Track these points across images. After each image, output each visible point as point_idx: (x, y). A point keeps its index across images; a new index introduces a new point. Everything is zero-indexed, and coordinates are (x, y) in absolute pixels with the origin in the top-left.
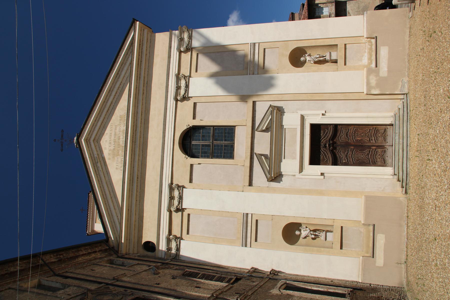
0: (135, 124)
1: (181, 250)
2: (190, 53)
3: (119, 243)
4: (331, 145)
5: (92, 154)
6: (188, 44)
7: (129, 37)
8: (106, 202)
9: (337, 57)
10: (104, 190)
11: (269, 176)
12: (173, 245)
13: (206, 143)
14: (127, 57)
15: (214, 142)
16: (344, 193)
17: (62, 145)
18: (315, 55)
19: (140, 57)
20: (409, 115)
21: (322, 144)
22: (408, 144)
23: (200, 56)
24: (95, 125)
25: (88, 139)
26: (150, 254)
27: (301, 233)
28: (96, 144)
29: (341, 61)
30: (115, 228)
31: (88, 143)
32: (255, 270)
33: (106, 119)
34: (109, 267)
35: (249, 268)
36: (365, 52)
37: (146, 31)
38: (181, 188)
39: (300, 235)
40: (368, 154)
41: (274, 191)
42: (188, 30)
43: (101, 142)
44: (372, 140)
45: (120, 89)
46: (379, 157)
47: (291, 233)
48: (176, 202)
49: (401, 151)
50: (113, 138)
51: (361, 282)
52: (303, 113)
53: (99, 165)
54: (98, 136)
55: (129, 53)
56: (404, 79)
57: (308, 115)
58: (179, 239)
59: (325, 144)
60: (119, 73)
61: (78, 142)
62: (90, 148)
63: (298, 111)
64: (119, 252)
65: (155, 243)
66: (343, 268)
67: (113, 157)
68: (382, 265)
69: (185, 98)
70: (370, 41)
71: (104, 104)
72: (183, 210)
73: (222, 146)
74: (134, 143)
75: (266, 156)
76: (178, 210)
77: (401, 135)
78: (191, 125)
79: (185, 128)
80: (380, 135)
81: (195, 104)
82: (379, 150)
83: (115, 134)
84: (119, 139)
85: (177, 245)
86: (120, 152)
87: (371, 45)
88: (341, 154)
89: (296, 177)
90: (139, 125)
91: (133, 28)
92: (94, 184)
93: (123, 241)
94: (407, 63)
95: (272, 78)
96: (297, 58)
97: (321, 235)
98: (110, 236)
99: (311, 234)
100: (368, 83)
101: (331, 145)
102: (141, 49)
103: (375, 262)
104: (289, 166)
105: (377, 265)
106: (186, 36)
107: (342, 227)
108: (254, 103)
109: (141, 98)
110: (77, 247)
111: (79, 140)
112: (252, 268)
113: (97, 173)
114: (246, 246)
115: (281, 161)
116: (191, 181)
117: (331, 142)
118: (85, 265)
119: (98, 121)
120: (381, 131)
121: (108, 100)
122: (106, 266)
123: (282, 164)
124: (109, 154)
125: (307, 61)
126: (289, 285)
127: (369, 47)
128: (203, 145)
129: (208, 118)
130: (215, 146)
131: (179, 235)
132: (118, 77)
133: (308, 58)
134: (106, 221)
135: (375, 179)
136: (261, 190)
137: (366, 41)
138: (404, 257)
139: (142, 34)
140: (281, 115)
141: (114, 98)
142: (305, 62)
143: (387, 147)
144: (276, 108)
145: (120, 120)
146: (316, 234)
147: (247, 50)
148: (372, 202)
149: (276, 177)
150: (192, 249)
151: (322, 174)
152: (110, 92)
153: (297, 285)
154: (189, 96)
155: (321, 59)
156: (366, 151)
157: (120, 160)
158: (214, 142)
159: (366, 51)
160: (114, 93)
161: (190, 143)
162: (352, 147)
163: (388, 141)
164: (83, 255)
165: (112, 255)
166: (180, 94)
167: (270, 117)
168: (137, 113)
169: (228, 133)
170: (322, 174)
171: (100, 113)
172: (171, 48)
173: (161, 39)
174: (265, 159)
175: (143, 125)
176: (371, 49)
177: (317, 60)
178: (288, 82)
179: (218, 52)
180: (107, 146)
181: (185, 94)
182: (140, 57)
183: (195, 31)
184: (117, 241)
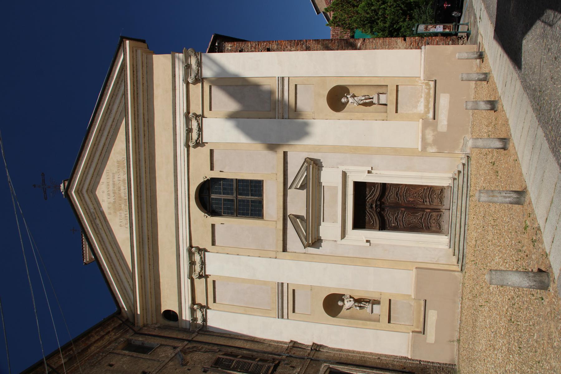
0: (138, 174)
1: (208, 320)
3: (134, 314)
4: (380, 206)
5: (87, 208)
6: (197, 74)
7: (118, 62)
8: (113, 267)
10: (108, 251)
11: (306, 243)
12: (199, 315)
13: (229, 197)
14: (118, 86)
15: (238, 196)
16: (393, 262)
18: (361, 94)
19: (135, 88)
20: (469, 189)
21: (368, 204)
22: (466, 223)
23: (213, 89)
24: (86, 173)
25: (80, 190)
26: (172, 323)
27: (344, 304)
28: (91, 195)
29: (391, 107)
30: (127, 296)
31: (81, 195)
32: (294, 345)
33: (99, 165)
34: (129, 356)
35: (288, 340)
36: (421, 97)
37: (139, 52)
40: (421, 218)
42: (195, 55)
43: (97, 193)
44: (426, 201)
45: (114, 127)
46: (434, 221)
48: (198, 268)
49: (459, 213)
50: (111, 188)
52: (344, 168)
53: (98, 221)
54: (92, 185)
55: (120, 82)
56: (466, 136)
57: (351, 172)
58: (204, 308)
59: (372, 205)
60: (110, 107)
61: (67, 189)
62: (83, 201)
63: (340, 167)
64: (136, 325)
65: (177, 312)
66: (392, 343)
67: (115, 212)
68: (433, 342)
69: (199, 144)
70: (428, 83)
71: (95, 147)
72: (207, 277)
73: (248, 201)
74: (139, 198)
76: (200, 277)
77: (459, 208)
78: (208, 178)
79: (202, 180)
80: (435, 196)
81: (212, 151)
82: (434, 214)
83: (114, 184)
84: (120, 190)
85: (203, 315)
86: (123, 206)
87: (429, 89)
88: (390, 217)
89: (338, 243)
90: (143, 175)
91: (121, 49)
92: (95, 246)
93: (139, 313)
94: (471, 117)
95: (306, 124)
96: (337, 98)
98: (123, 306)
99: (356, 306)
100: (424, 139)
101: (380, 206)
102: (135, 77)
103: (426, 339)
104: (329, 230)
105: (428, 341)
106: (193, 61)
107: (390, 300)
108: (285, 154)
109: (142, 141)
110: (87, 334)
111: (69, 192)
112: (291, 341)
113: (97, 232)
114: (283, 317)
115: (319, 224)
116: (213, 243)
117: (378, 203)
118: (100, 358)
119: (90, 168)
120: (437, 192)
121: (99, 142)
122: (124, 355)
123: (321, 228)
124: (109, 208)
126: (333, 370)
127: (427, 91)
128: (225, 200)
129: (231, 170)
130: (240, 201)
131: (204, 304)
132: (108, 112)
134: (115, 290)
136: (297, 257)
137: (423, 83)
138: (457, 335)
139: (135, 57)
140: (319, 170)
141: (107, 138)
143: (443, 210)
144: (312, 162)
145: (119, 166)
146: (362, 305)
147: (273, 85)
148: (424, 272)
152: (101, 132)
153: (340, 369)
154: (204, 141)
155: (367, 101)
156: (419, 214)
157: (123, 215)
158: (238, 196)
159: (423, 95)
160: (105, 134)
161: (209, 196)
162: (403, 209)
163: (445, 204)
164: (95, 342)
165: (128, 330)
167: (306, 174)
168: (139, 161)
169: (255, 187)
171: (92, 158)
172: (175, 90)
173: (161, 63)
174: (301, 222)
175: (148, 175)
176: (428, 94)
177: (362, 102)
178: (326, 132)
179: (237, 86)
180: (105, 198)
181: (198, 139)
182: (135, 88)
183: (205, 55)
184: (131, 311)
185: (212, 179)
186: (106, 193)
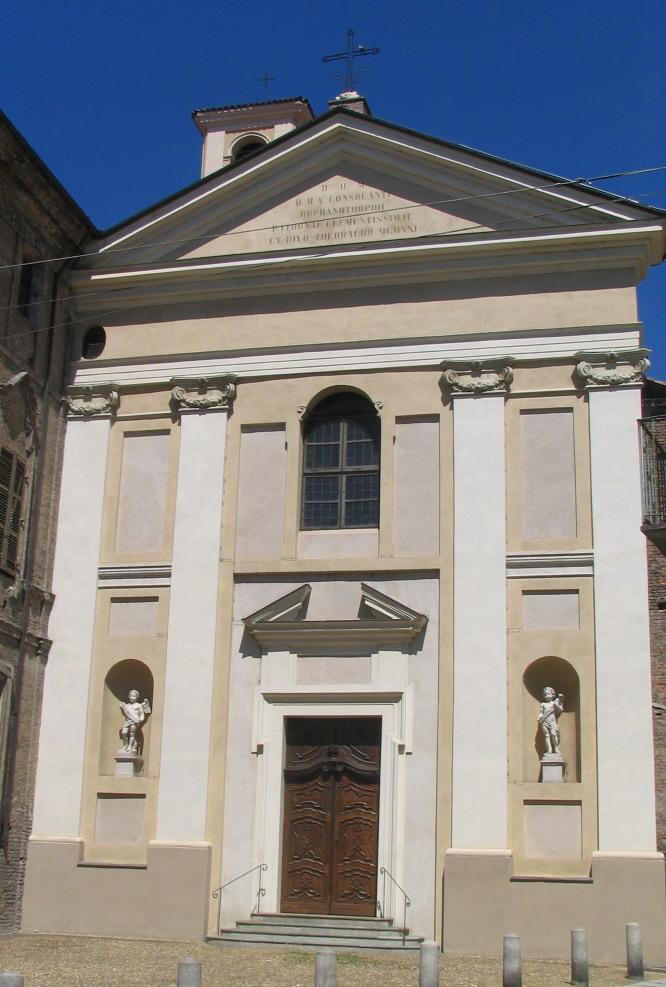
2: (574, 388)
4: (332, 762)
9: (47, 945)
15: (344, 477)
17: (338, 57)
26: (79, 344)
35: (55, 590)
38: (228, 405)
39: (128, 701)
41: (223, 635)
47: (131, 679)
51: (31, 837)
52: (408, 698)
58: (112, 413)
64: (73, 272)
65: (103, 356)
66: (58, 805)
69: (449, 392)
72: (176, 416)
75: (303, 611)
76: (175, 404)
78: (381, 413)
79: (374, 398)
81: (434, 418)
93: (93, 278)
97: (129, 748)
101: (332, 762)
104: (283, 669)
107: (143, 796)
112: (53, 597)
114: (102, 577)
116: (247, 428)
124: (310, 201)
125: (543, 704)
129: (400, 457)
133: (549, 706)
135: (253, 873)
136: (225, 603)
142: (542, 699)
146: (132, 739)
148: (194, 867)
149: (257, 640)
150: (85, 450)
151: (260, 749)
155: (548, 740)
158: (344, 477)
162: (328, 820)
164: (37, 201)
166: (460, 375)
167: (394, 617)
169: (365, 512)
170: (260, 749)
173: (621, 303)
181: (461, 388)
185: (377, 422)
186: (343, 192)
